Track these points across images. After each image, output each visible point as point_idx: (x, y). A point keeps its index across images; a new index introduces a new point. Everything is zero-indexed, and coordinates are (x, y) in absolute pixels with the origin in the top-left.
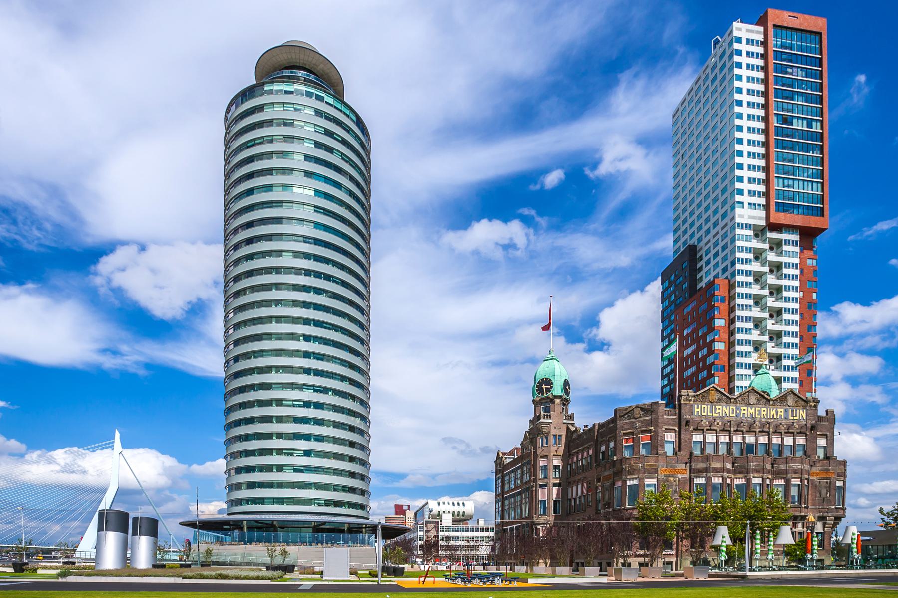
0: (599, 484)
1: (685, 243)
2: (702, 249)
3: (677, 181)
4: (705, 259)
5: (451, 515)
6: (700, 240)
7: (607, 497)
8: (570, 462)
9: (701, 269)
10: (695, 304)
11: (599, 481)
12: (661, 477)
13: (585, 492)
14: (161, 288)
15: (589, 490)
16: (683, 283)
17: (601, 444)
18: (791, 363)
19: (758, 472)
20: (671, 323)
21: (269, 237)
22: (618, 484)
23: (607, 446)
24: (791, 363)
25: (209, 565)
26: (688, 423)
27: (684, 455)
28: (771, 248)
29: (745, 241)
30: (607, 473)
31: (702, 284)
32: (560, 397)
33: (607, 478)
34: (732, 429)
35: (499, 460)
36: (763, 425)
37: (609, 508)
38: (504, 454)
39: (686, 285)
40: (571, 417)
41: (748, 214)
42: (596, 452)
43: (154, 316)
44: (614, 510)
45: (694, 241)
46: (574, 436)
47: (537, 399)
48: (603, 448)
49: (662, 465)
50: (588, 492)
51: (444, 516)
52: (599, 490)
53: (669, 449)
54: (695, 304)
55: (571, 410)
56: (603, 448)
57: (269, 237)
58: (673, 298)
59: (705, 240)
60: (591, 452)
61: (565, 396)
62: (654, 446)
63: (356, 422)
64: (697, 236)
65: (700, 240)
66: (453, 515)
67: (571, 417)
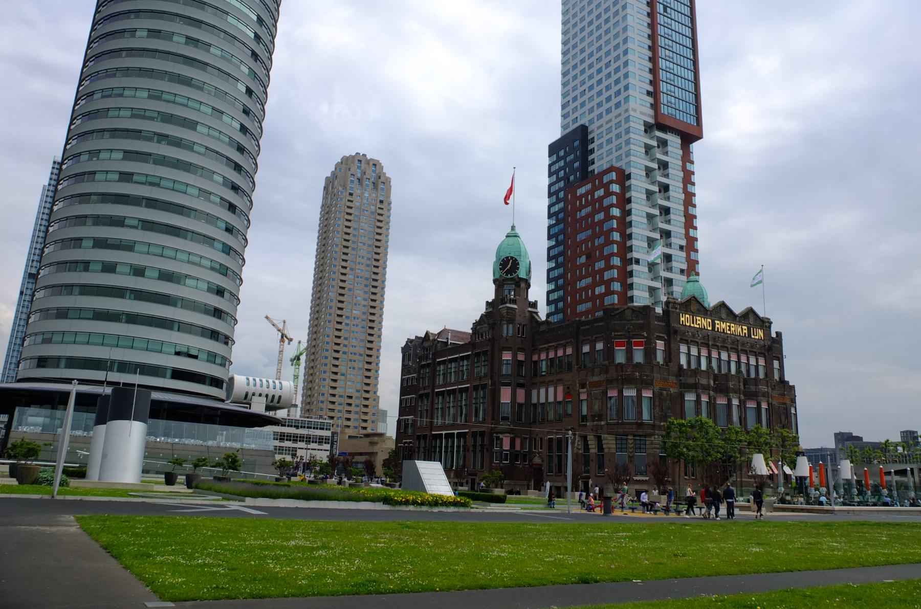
2: (593, 131)
3: (567, 57)
6: (591, 121)
9: (592, 151)
10: (589, 186)
11: (583, 386)
12: (657, 389)
15: (567, 394)
16: (574, 161)
17: (584, 343)
19: (736, 392)
20: (558, 201)
23: (593, 348)
25: (40, 483)
26: (676, 332)
28: (658, 147)
30: (596, 379)
33: (597, 384)
34: (710, 343)
36: (733, 343)
39: (577, 164)
41: (639, 109)
42: (578, 350)
44: (608, 424)
49: (657, 376)
51: (255, 399)
54: (589, 186)
58: (562, 173)
59: (597, 124)
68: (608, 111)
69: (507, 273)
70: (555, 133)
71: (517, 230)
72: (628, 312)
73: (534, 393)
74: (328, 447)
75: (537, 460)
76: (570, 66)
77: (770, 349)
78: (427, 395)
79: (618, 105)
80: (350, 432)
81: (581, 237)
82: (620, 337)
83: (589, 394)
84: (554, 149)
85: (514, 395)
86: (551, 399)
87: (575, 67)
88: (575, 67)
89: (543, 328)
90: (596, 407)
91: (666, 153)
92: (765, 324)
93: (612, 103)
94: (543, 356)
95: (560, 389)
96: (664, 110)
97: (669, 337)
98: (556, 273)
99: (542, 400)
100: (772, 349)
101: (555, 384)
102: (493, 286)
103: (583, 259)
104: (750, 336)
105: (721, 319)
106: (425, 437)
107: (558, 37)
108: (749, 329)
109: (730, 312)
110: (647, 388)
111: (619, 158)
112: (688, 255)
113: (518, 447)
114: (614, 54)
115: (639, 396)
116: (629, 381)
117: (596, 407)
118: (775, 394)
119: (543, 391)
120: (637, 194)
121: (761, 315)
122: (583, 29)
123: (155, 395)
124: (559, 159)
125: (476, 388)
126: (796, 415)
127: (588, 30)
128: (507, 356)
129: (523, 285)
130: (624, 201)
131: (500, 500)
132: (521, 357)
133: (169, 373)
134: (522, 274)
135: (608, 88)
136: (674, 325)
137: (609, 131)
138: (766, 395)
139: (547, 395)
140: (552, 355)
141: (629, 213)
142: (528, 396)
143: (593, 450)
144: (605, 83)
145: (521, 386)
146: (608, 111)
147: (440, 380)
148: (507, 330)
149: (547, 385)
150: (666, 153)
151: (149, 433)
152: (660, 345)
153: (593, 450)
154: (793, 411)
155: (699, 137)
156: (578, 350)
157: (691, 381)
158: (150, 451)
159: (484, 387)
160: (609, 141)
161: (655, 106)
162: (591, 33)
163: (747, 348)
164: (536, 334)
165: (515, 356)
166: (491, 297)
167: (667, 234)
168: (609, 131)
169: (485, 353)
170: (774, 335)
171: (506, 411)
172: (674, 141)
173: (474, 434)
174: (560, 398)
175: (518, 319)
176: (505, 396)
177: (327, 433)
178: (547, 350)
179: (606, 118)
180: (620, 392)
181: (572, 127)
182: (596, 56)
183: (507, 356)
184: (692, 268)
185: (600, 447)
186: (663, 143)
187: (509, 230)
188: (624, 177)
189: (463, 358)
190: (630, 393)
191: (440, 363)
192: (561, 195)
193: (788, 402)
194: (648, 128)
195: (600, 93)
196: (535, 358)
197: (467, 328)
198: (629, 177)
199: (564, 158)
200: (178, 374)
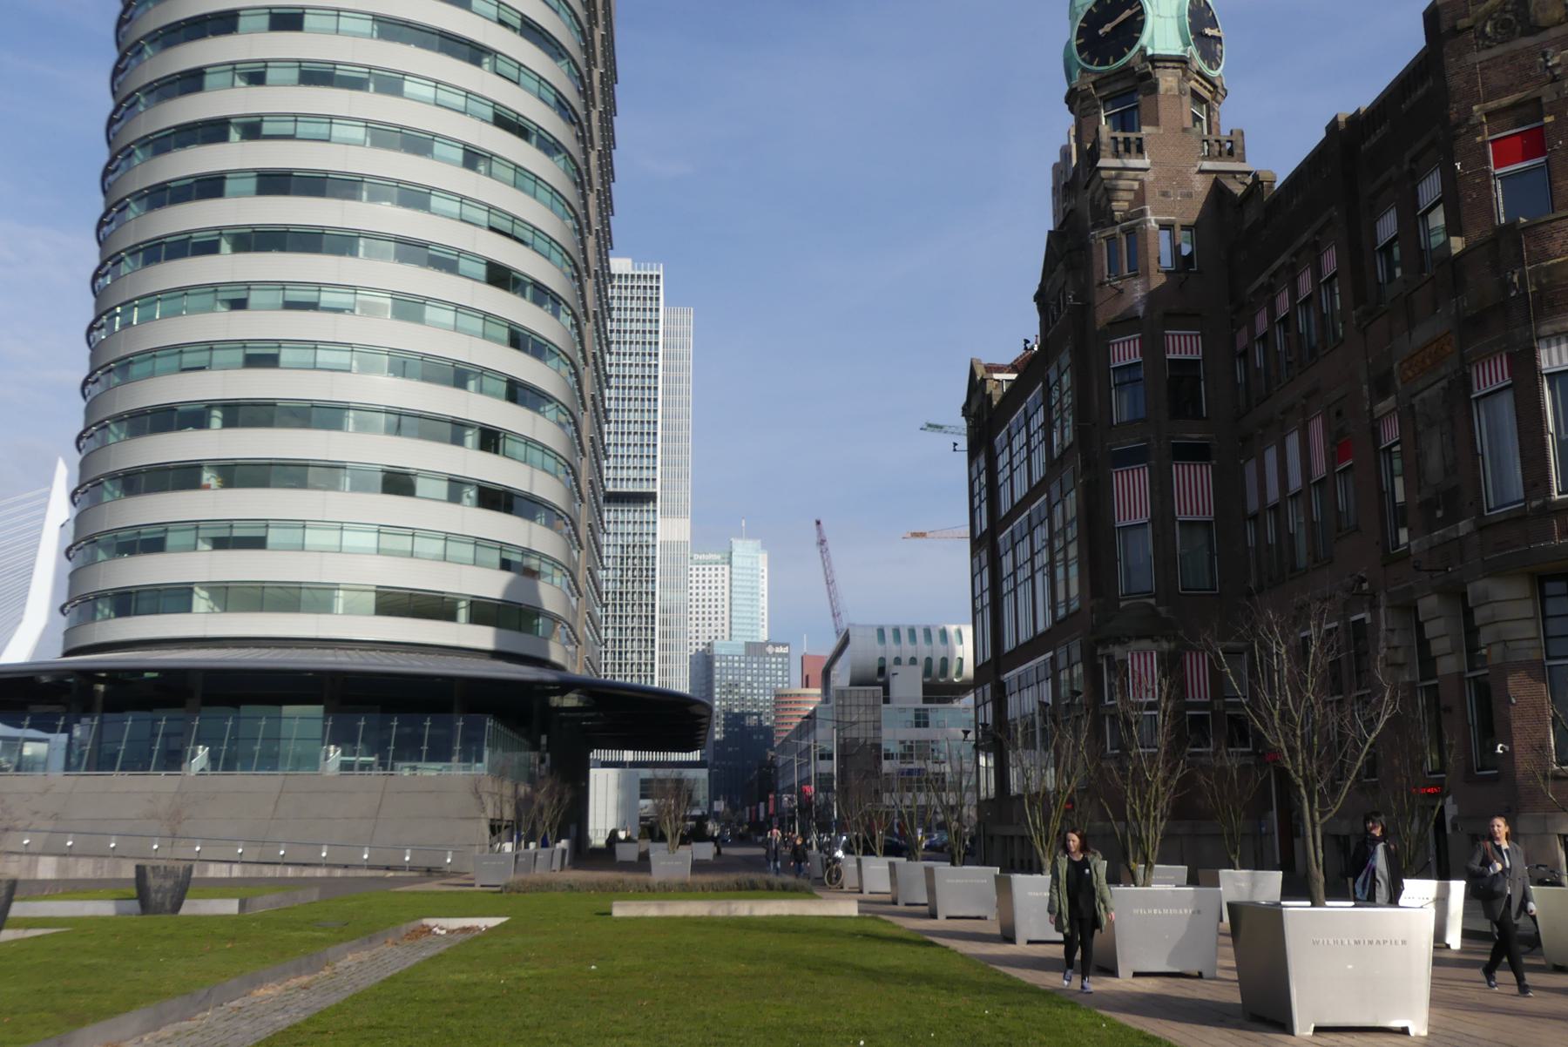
0: (1382, 407)
5: (919, 670)
7: (1434, 462)
8: (1242, 340)
11: (1382, 387)
13: (1320, 469)
14: (915, 535)
15: (1339, 447)
18: (1441, 630)
22: (1492, 376)
24: (1441, 630)
30: (1422, 335)
32: (1182, 61)
35: (976, 386)
37: (1452, 518)
38: (991, 369)
40: (1231, 149)
42: (1358, 250)
44: (1483, 527)
46: (1252, 214)
47: (1087, 84)
48: (1388, 226)
50: (1332, 461)
52: (1391, 433)
55: (1228, 117)
60: (1330, 262)
61: (1198, 63)
66: (928, 672)
67: (1231, 149)
85: (1162, 492)
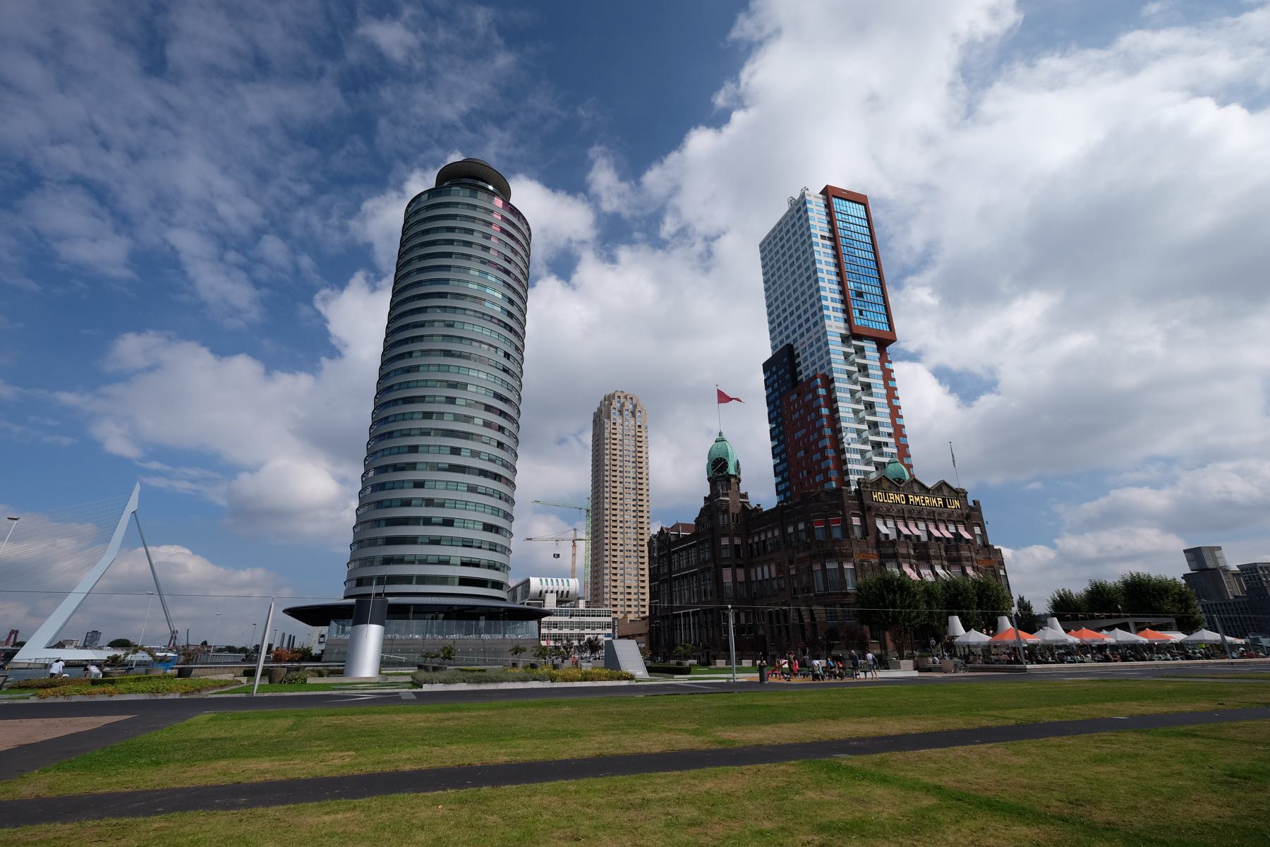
1: (781, 342)
4: (802, 357)
6: (795, 341)
9: (799, 364)
11: (791, 562)
12: (857, 561)
15: (779, 571)
21: (467, 218)
23: (796, 528)
26: (869, 508)
27: (871, 539)
29: (837, 349)
30: (801, 555)
31: (803, 377)
37: (809, 592)
41: (835, 326)
42: (784, 532)
43: (696, 128)
45: (790, 341)
48: (791, 530)
49: (856, 549)
53: (857, 533)
56: (791, 530)
57: (467, 218)
62: (847, 528)
63: (502, 505)
64: (793, 337)
65: (795, 341)
68: (808, 330)
69: (718, 471)
70: (768, 354)
71: (724, 436)
72: (823, 495)
73: (753, 571)
74: (544, 631)
75: (761, 632)
76: (772, 299)
77: (968, 517)
78: (666, 581)
79: (816, 324)
80: (631, 617)
81: (799, 434)
82: (818, 517)
83: (797, 570)
84: (767, 366)
85: (734, 575)
86: (767, 576)
87: (776, 299)
88: (776, 299)
89: (753, 515)
90: (804, 580)
91: (864, 357)
92: (960, 494)
93: (811, 323)
94: (756, 539)
95: (773, 567)
96: (857, 322)
97: (863, 511)
98: (781, 467)
99: (760, 578)
100: (972, 515)
101: (768, 562)
102: (708, 484)
103: (802, 453)
104: (945, 506)
105: (915, 494)
106: (667, 617)
107: (761, 278)
108: (944, 500)
109: (922, 487)
110: (848, 561)
111: (822, 367)
112: (897, 441)
113: (743, 621)
114: (807, 284)
115: (841, 569)
116: (831, 555)
117: (804, 580)
118: (980, 557)
119: (759, 569)
120: (842, 396)
121: (955, 486)
122: (779, 269)
123: (391, 600)
124: (772, 374)
125: (702, 571)
126: (1006, 576)
127: (783, 269)
128: (725, 541)
129: (733, 480)
130: (832, 401)
131: (686, 671)
132: (737, 541)
133: (457, 581)
134: (732, 471)
135: (806, 312)
136: (867, 502)
137: (811, 345)
138: (970, 559)
139: (764, 572)
140: (763, 537)
141: (837, 410)
142: (748, 575)
143: (807, 620)
144: (803, 308)
145: (740, 566)
146: (808, 330)
147: (675, 568)
148: (723, 519)
149: (762, 564)
150: (864, 357)
151: (386, 632)
152: (856, 521)
153: (807, 620)
154: (1002, 573)
155: (893, 340)
156: (784, 532)
157: (890, 551)
158: (387, 646)
159: (709, 569)
160: (812, 354)
161: (848, 320)
162: (786, 271)
163: (944, 517)
164: (752, 518)
165: (731, 541)
166: (707, 493)
167: (874, 426)
168: (811, 345)
169: (706, 541)
170: (971, 504)
171: (729, 592)
172: (870, 347)
173: (705, 612)
174: (774, 575)
175: (731, 510)
176: (727, 575)
177: (610, 619)
178: (759, 534)
179: (807, 336)
180: (823, 566)
181: (780, 347)
182: (793, 288)
183: (725, 541)
184: (903, 451)
185: (813, 618)
186: (860, 351)
187: (717, 437)
188: (829, 382)
189: (691, 547)
190: (832, 566)
191: (674, 552)
192: (778, 402)
193: (996, 565)
194: (845, 340)
195: (799, 317)
196: (750, 541)
197: (691, 520)
198: (832, 381)
199: (776, 372)
200: (464, 581)
